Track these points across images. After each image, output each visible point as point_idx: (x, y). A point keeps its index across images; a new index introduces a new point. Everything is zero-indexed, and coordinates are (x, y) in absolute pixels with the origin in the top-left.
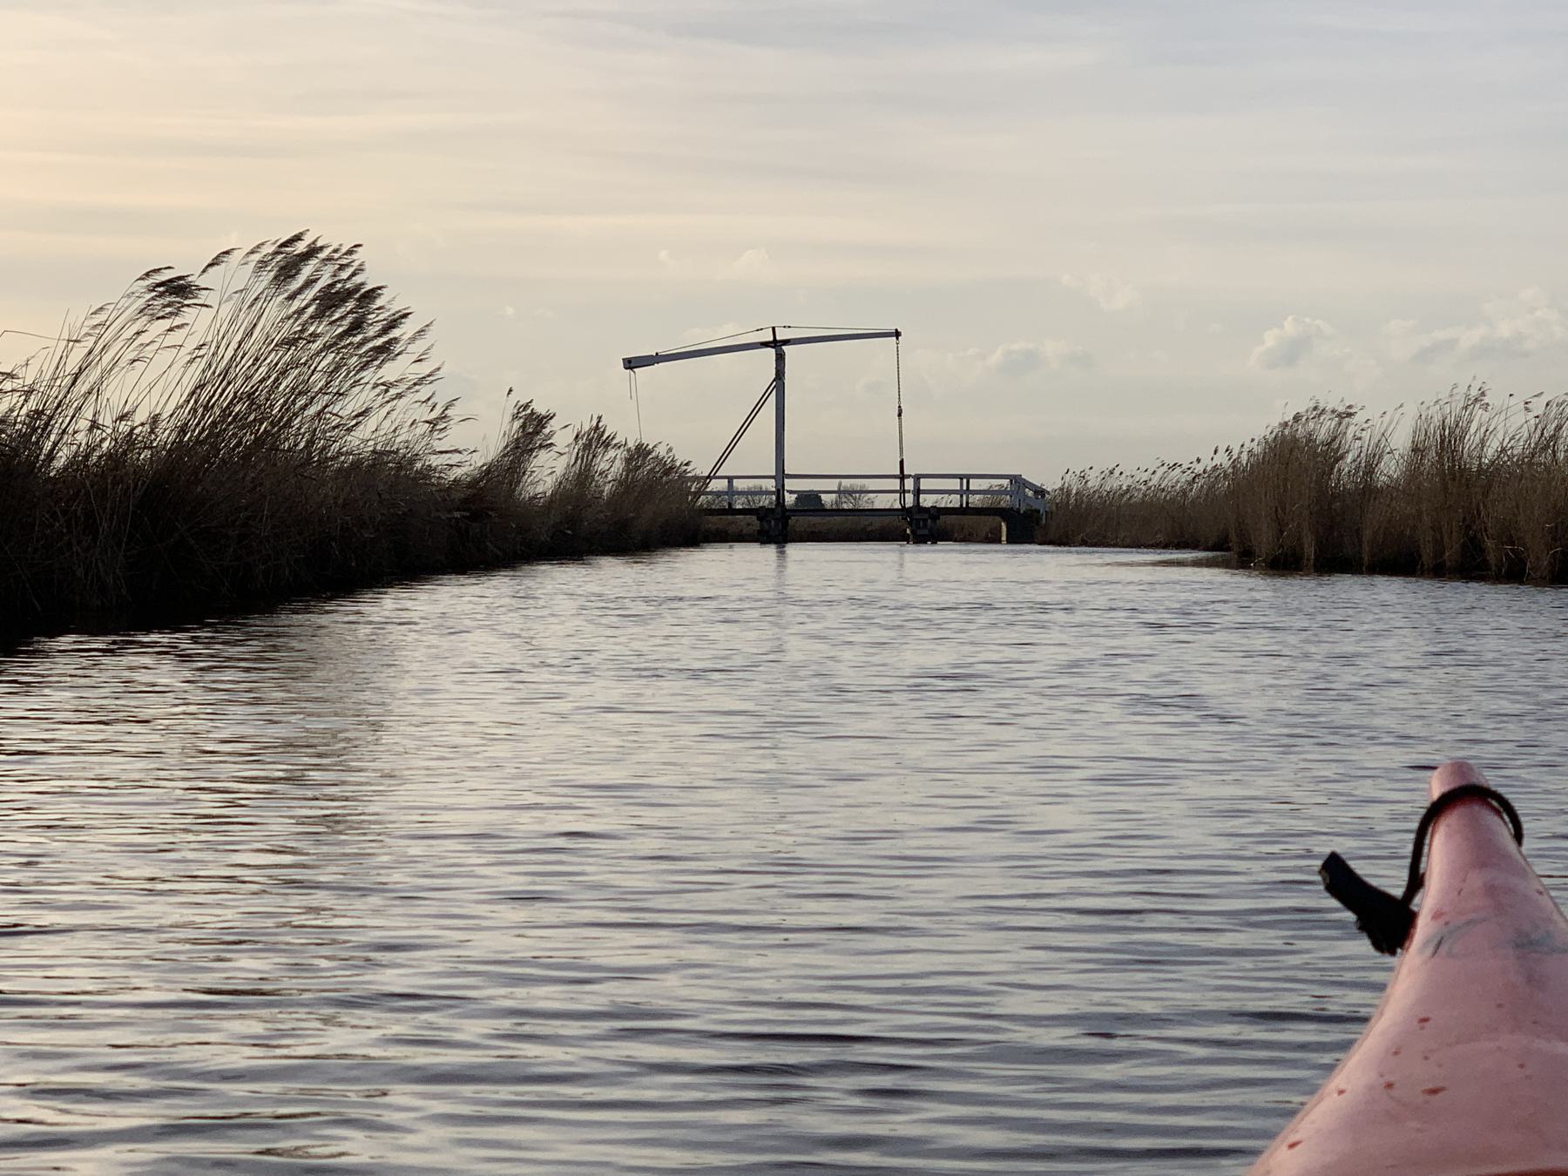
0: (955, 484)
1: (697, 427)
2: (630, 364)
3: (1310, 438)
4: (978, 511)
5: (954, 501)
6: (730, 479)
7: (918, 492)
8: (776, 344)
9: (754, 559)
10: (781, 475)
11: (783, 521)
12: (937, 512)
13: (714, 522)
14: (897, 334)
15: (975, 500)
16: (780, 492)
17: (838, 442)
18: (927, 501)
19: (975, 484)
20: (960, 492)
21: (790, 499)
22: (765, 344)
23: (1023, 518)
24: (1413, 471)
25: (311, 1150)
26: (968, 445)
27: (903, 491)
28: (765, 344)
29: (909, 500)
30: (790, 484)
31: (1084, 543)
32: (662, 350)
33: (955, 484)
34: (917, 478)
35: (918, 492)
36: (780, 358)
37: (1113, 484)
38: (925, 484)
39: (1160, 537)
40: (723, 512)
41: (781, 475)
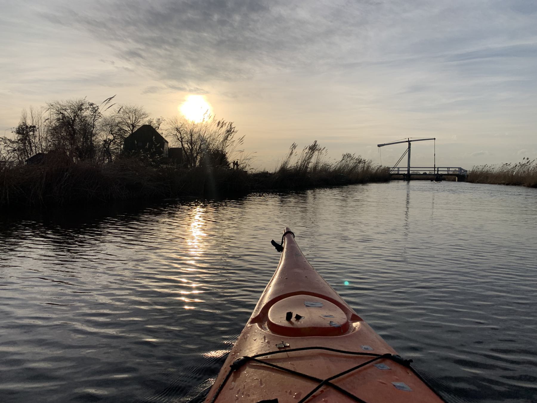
0: (446, 169)
1: (378, 160)
2: (379, 146)
3: (348, 165)
4: (451, 175)
5: (446, 173)
6: (398, 168)
7: (398, 171)
8: (409, 141)
9: (402, 184)
10: (409, 167)
11: (408, 177)
12: (442, 175)
13: (396, 177)
14: (435, 139)
15: (451, 173)
16: (409, 171)
17: (421, 161)
18: (440, 173)
19: (450, 169)
20: (447, 171)
21: (411, 172)
22: (407, 141)
23: (461, 176)
24: (333, 172)
25: (483, 290)
26: (447, 162)
27: (435, 171)
28: (407, 141)
29: (436, 172)
30: (411, 169)
31: (478, 182)
32: (386, 143)
33: (446, 169)
34: (438, 168)
35: (438, 171)
36: (410, 144)
37: (485, 170)
38: (439, 169)
39: (503, 182)
40: (396, 174)
41: (409, 167)
